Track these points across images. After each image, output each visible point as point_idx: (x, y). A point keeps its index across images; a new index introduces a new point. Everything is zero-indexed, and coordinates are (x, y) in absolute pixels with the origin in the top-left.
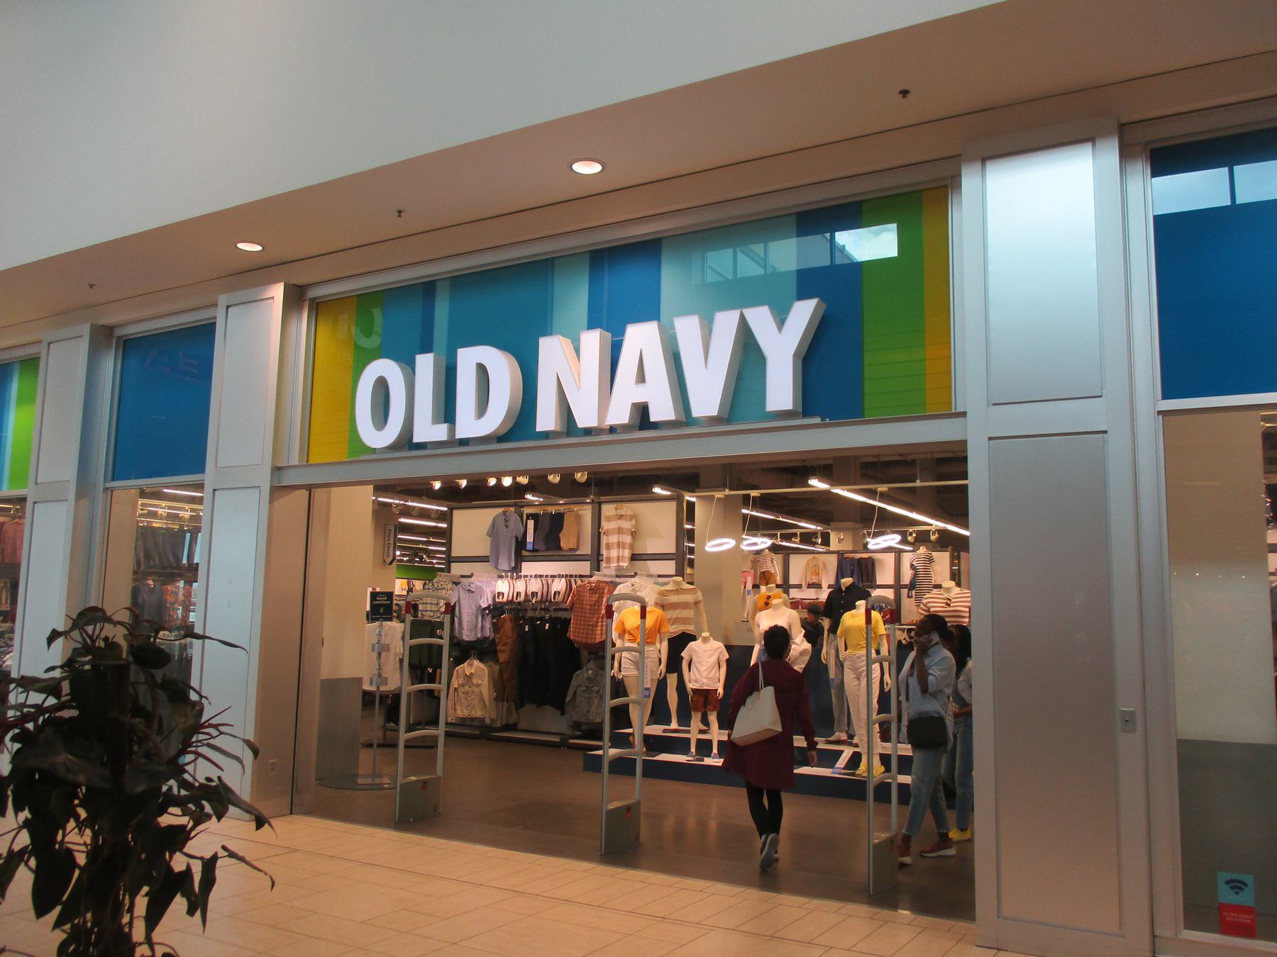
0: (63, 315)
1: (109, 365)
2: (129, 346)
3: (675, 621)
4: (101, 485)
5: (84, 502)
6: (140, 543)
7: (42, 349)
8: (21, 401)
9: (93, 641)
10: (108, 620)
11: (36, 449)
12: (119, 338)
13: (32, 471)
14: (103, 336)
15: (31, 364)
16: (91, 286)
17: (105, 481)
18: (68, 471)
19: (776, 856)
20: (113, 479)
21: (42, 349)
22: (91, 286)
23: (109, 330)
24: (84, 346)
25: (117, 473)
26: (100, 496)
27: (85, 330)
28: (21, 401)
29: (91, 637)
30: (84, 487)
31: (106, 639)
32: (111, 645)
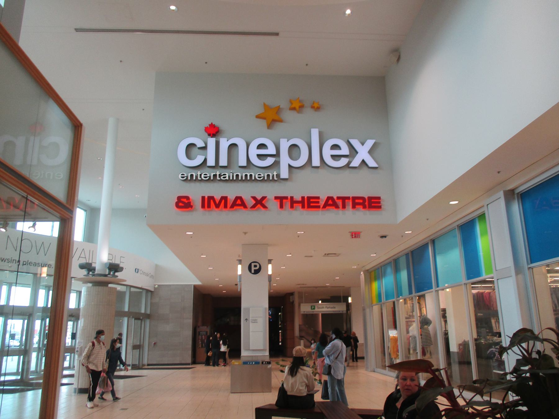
0: (490, 191)
1: (516, 207)
2: (524, 196)
3: (408, 325)
4: (526, 267)
5: (520, 276)
6: (554, 296)
7: (485, 209)
8: (482, 235)
9: (530, 354)
10: (536, 338)
11: (492, 255)
12: (518, 193)
13: (493, 266)
14: (510, 195)
15: (482, 217)
16: (499, 172)
17: (528, 264)
18: (510, 263)
19: (289, 197)
20: (531, 263)
21: (485, 209)
22: (499, 172)
23: (512, 191)
24: (502, 203)
25: (533, 258)
26: (527, 272)
27: (501, 194)
28: (482, 235)
29: (527, 351)
30: (518, 269)
31: (538, 352)
32: (543, 357)
